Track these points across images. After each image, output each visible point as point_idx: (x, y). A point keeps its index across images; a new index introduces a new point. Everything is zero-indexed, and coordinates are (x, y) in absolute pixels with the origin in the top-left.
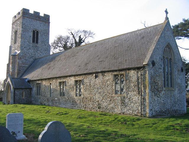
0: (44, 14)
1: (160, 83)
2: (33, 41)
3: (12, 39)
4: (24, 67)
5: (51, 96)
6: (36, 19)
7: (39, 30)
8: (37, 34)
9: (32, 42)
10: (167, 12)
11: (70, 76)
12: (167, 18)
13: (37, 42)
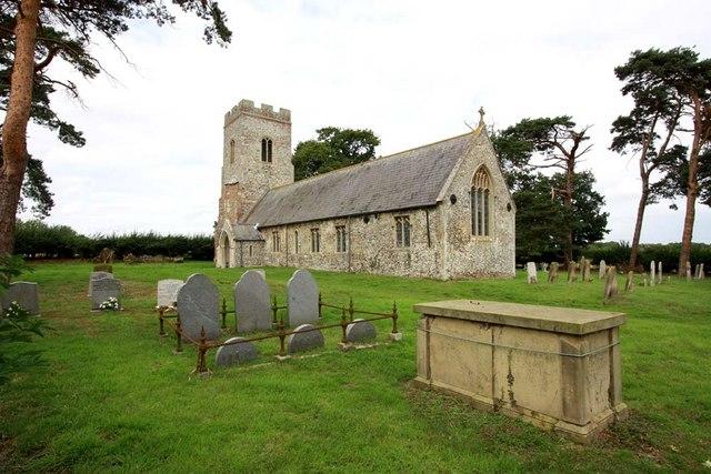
0: (263, 105)
1: (466, 229)
2: (264, 159)
3: (225, 156)
10: (482, 112)
11: (327, 219)
12: (481, 123)
13: (270, 160)
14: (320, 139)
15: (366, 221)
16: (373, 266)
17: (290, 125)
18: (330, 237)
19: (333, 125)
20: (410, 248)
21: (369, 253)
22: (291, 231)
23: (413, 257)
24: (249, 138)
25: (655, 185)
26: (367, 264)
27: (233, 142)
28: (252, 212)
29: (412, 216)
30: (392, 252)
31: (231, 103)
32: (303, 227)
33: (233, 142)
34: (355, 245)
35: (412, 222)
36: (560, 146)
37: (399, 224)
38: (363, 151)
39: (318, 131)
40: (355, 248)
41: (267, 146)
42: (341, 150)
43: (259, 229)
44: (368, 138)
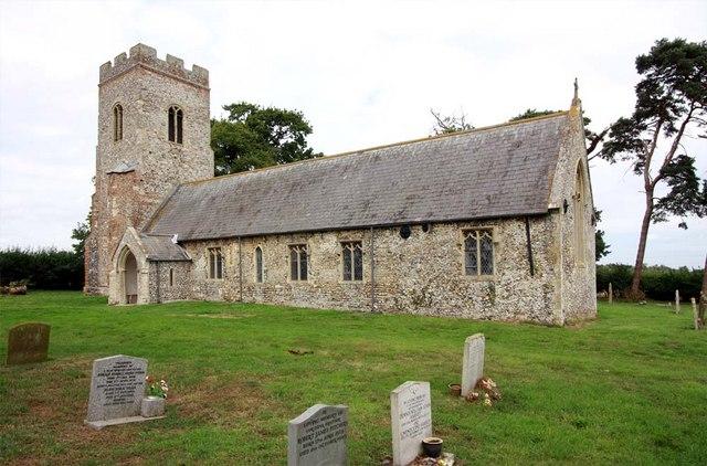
2: (171, 138)
3: (102, 129)
4: (150, 204)
5: (260, 279)
6: (174, 79)
7: (184, 107)
8: (180, 119)
9: (167, 139)
11: (323, 231)
12: (576, 102)
13: (180, 141)
14: (232, 117)
15: (405, 235)
16: (417, 302)
17: (209, 91)
18: (328, 258)
19: (249, 101)
20: (495, 276)
21: (410, 283)
22: (249, 249)
23: (499, 290)
24: (150, 103)
25: (663, 201)
26: (406, 300)
27: (118, 110)
28: (156, 217)
29: (496, 229)
30: (455, 283)
31: (117, 46)
32: (272, 242)
33: (118, 110)
34: (381, 270)
35: (497, 238)
36: (181, 185)
37: (471, 243)
38: (288, 139)
39: (227, 108)
40: (384, 276)
41: (176, 118)
42: (259, 139)
43: (180, 243)
44: (295, 122)
